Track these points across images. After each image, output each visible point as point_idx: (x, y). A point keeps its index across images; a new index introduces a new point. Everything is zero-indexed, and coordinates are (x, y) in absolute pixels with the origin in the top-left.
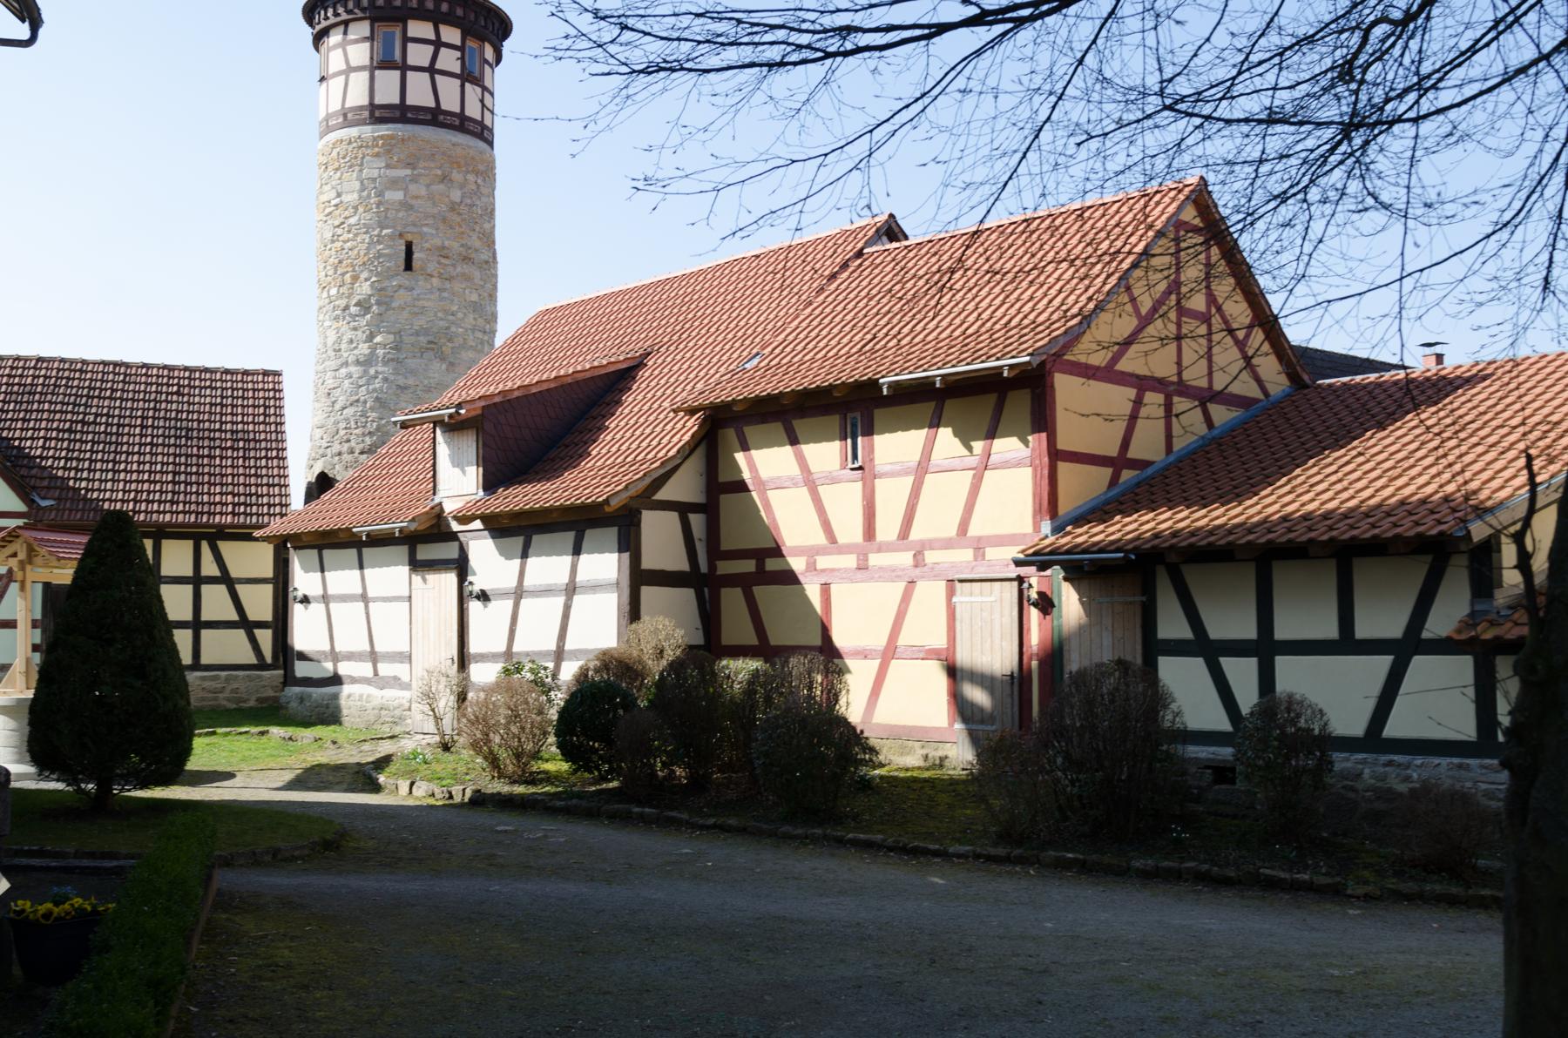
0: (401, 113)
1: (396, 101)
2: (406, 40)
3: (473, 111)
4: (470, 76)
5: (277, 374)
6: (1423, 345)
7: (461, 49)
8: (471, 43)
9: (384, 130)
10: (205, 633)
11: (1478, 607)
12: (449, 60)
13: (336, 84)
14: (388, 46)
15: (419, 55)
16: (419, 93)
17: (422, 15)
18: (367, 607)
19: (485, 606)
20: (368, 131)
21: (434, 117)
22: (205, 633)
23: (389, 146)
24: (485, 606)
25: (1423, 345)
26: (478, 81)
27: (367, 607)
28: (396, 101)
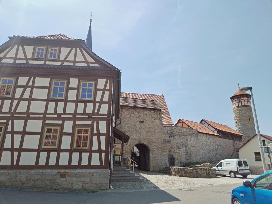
0: (242, 106)
1: (241, 105)
2: (241, 99)
3: (249, 105)
4: (248, 101)
5: (180, 120)
6: (178, 200)
7: (247, 99)
8: (248, 98)
9: (240, 108)
10: (26, 136)
11: (161, 121)
12: (246, 100)
13: (234, 105)
14: (239, 100)
15: (243, 101)
16: (243, 104)
17: (242, 97)
18: (242, 105)
19: (140, 141)
20: (237, 109)
21: (245, 106)
22: (26, 136)
23: (238, 110)
24: (140, 141)
25: (178, 200)
26: (249, 102)
27: (242, 105)
28: (241, 105)
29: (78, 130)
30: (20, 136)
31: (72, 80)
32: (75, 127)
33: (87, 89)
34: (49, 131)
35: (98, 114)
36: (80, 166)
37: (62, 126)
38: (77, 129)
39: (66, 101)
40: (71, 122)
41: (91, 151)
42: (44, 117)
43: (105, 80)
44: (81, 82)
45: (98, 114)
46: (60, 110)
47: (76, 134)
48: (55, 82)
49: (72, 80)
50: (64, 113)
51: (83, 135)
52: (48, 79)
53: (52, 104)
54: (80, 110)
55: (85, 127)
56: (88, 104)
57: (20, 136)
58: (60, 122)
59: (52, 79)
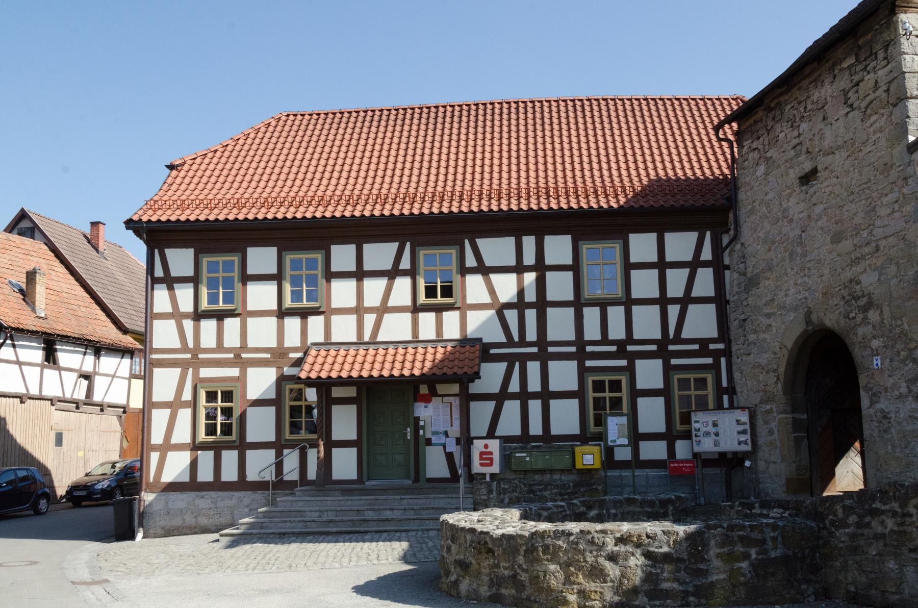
29: (619, 382)
30: (167, 412)
31: (335, 249)
32: (585, 374)
33: (304, 276)
34: (599, 386)
35: (678, 340)
36: (217, 485)
37: (630, 370)
38: (590, 380)
39: (628, 302)
40: (658, 364)
41: (243, 446)
42: (278, 354)
43: (395, 246)
44: (419, 253)
45: (678, 340)
46: (617, 331)
47: (591, 395)
48: (208, 262)
49: (335, 249)
50: (244, 347)
51: (693, 393)
52: (273, 251)
53: (591, 315)
54: (592, 331)
55: (609, 373)
56: (445, 314)
57: (167, 412)
58: (623, 363)
59: (200, 255)
